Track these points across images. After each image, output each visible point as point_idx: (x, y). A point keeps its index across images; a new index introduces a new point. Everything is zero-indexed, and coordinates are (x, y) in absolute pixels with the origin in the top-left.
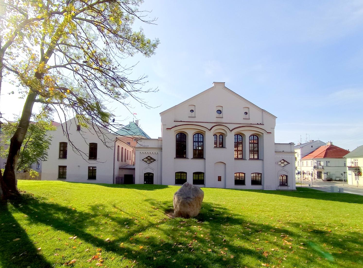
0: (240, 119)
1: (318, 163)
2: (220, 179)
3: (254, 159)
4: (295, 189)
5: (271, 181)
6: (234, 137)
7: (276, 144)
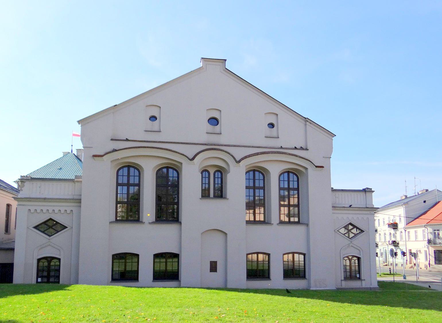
0: (259, 137)
1: (435, 233)
2: (213, 267)
3: (255, 222)
4: (375, 285)
5: (325, 271)
6: (244, 177)
7: (333, 190)
